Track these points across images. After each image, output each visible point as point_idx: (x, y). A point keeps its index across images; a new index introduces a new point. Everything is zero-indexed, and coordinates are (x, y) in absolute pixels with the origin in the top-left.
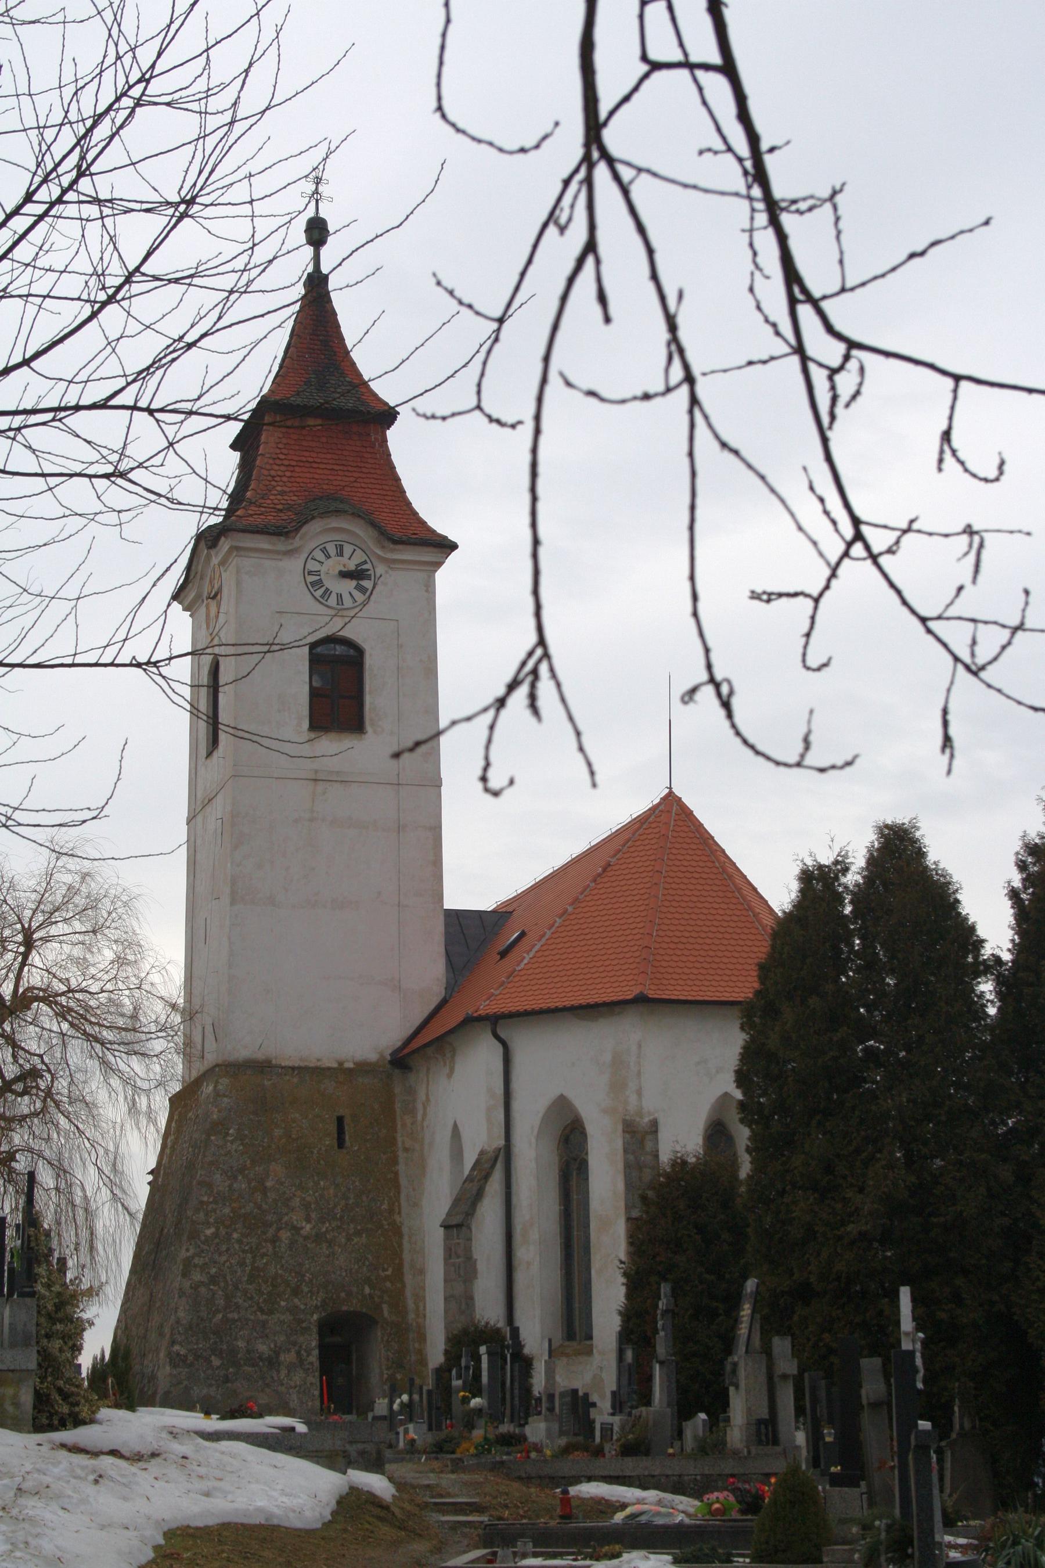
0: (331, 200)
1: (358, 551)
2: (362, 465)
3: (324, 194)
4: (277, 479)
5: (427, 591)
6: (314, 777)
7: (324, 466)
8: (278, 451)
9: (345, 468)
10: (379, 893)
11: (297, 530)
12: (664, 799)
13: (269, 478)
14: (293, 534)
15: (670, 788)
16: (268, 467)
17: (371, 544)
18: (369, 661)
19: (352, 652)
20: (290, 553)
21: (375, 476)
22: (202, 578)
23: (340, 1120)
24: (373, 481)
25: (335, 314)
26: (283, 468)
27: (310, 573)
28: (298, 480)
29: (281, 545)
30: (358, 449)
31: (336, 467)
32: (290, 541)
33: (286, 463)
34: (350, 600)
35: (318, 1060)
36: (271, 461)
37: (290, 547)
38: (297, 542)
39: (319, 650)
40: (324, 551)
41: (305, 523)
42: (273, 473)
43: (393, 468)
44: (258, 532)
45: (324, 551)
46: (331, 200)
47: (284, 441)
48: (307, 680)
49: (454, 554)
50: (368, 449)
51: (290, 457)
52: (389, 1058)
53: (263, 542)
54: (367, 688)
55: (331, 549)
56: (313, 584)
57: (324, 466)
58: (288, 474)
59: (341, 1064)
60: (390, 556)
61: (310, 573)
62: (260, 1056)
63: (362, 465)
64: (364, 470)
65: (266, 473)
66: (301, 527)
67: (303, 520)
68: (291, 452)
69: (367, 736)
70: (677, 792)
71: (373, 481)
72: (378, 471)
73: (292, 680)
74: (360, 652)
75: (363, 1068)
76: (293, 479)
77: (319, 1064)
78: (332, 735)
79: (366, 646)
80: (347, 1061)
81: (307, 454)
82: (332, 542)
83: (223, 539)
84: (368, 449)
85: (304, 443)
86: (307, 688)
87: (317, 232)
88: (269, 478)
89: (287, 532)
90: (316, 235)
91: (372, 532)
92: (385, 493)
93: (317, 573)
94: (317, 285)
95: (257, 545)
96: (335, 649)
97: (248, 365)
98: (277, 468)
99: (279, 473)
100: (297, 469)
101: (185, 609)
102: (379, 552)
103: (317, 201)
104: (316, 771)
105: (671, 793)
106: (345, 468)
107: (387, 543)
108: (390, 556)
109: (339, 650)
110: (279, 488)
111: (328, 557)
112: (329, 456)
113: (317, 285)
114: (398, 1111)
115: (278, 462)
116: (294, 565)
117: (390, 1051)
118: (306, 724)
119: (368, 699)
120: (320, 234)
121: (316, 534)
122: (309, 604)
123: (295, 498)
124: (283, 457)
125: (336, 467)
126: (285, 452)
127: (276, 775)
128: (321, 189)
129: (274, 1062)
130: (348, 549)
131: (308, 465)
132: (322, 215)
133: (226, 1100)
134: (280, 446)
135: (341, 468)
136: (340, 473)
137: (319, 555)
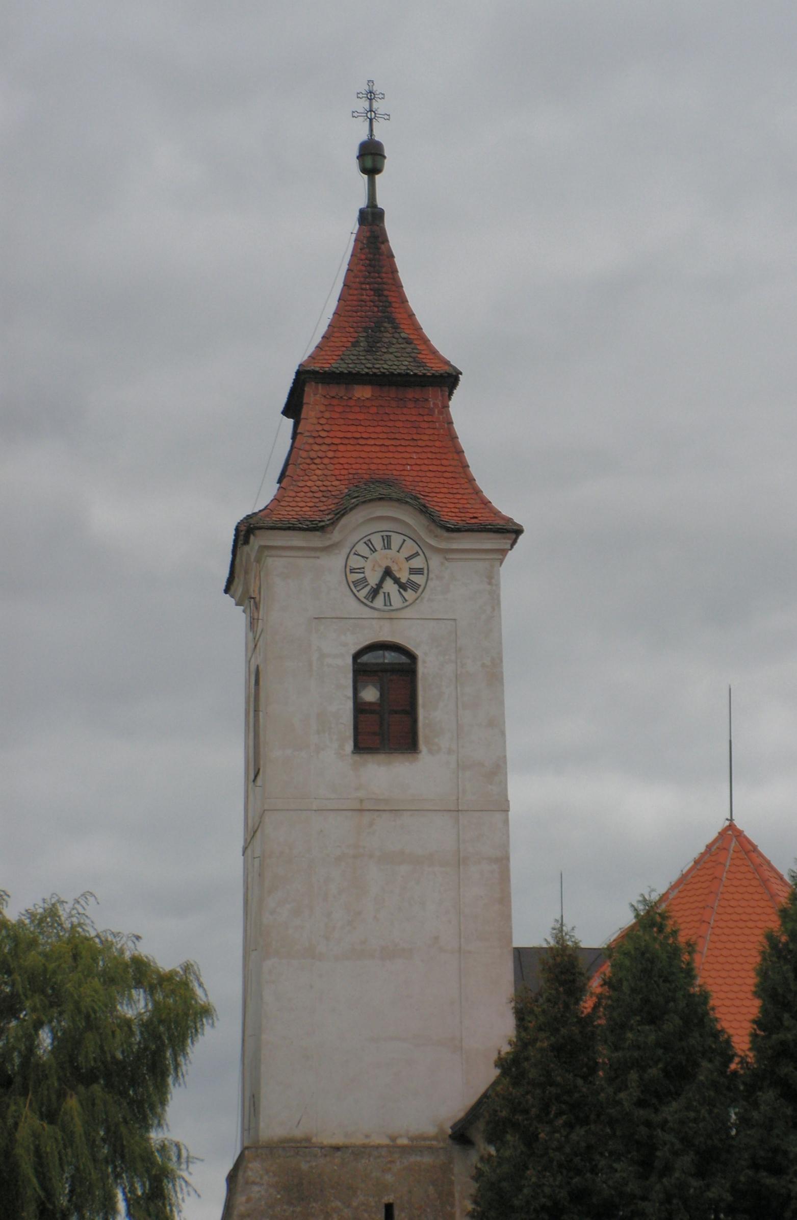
0: (387, 117)
1: (408, 541)
2: (418, 437)
3: (379, 111)
4: (318, 461)
5: (490, 583)
6: (358, 807)
7: (372, 442)
8: (319, 428)
9: (398, 442)
10: (437, 938)
11: (334, 523)
12: (722, 834)
13: (308, 461)
14: (331, 528)
15: (731, 820)
16: (307, 447)
17: (423, 534)
18: (421, 670)
19: (404, 659)
20: (327, 549)
21: (433, 450)
22: (246, 573)
23: (389, 1208)
24: (430, 455)
25: (392, 256)
26: (324, 448)
27: (352, 571)
28: (342, 461)
29: (315, 539)
30: (414, 418)
31: (387, 442)
32: (328, 536)
33: (328, 441)
34: (400, 599)
35: (367, 1136)
36: (311, 441)
37: (327, 543)
38: (336, 535)
39: (365, 659)
40: (369, 544)
41: (343, 515)
42: (312, 454)
43: (454, 438)
44: (289, 529)
45: (369, 544)
46: (387, 117)
47: (327, 415)
48: (350, 693)
49: (521, 538)
50: (426, 418)
51: (331, 434)
52: (450, 1131)
53: (296, 540)
54: (421, 700)
55: (377, 541)
56: (356, 583)
57: (372, 442)
58: (330, 454)
59: (393, 1139)
60: (443, 545)
61: (352, 571)
62: (298, 1133)
63: (418, 437)
64: (420, 443)
65: (304, 454)
66: (339, 519)
67: (340, 514)
68: (335, 428)
69: (420, 756)
70: (739, 824)
71: (430, 455)
72: (437, 444)
73: (334, 700)
74: (413, 658)
75: (417, 1145)
76: (336, 461)
77: (366, 1141)
78: (381, 757)
79: (418, 652)
80: (401, 1136)
81: (353, 428)
82: (374, 537)
83: (252, 538)
84: (426, 418)
85: (351, 416)
86: (350, 704)
87: (371, 158)
88: (308, 461)
89: (323, 527)
90: (369, 164)
91: (423, 520)
92: (444, 469)
93: (361, 570)
94: (371, 218)
95: (290, 543)
96: (384, 657)
97: (306, 316)
98: (316, 447)
99: (320, 454)
100: (341, 448)
101: (237, 604)
102: (433, 542)
103: (371, 120)
104: (361, 801)
105: (731, 827)
106: (398, 442)
107: (439, 531)
108: (443, 545)
109: (390, 657)
110: (319, 472)
111: (374, 550)
112: (378, 429)
113: (371, 218)
114: (457, 1195)
115: (319, 441)
116: (336, 562)
117: (450, 1123)
118: (349, 746)
119: (422, 714)
120: (374, 161)
121: (358, 526)
122: (352, 606)
123: (337, 483)
124: (323, 434)
125: (387, 442)
126: (327, 427)
127: (315, 808)
128: (375, 105)
129: (314, 1140)
130: (396, 540)
131: (352, 442)
132: (378, 137)
133: (256, 1188)
134: (323, 421)
135: (393, 442)
136: (391, 448)
137: (362, 549)
